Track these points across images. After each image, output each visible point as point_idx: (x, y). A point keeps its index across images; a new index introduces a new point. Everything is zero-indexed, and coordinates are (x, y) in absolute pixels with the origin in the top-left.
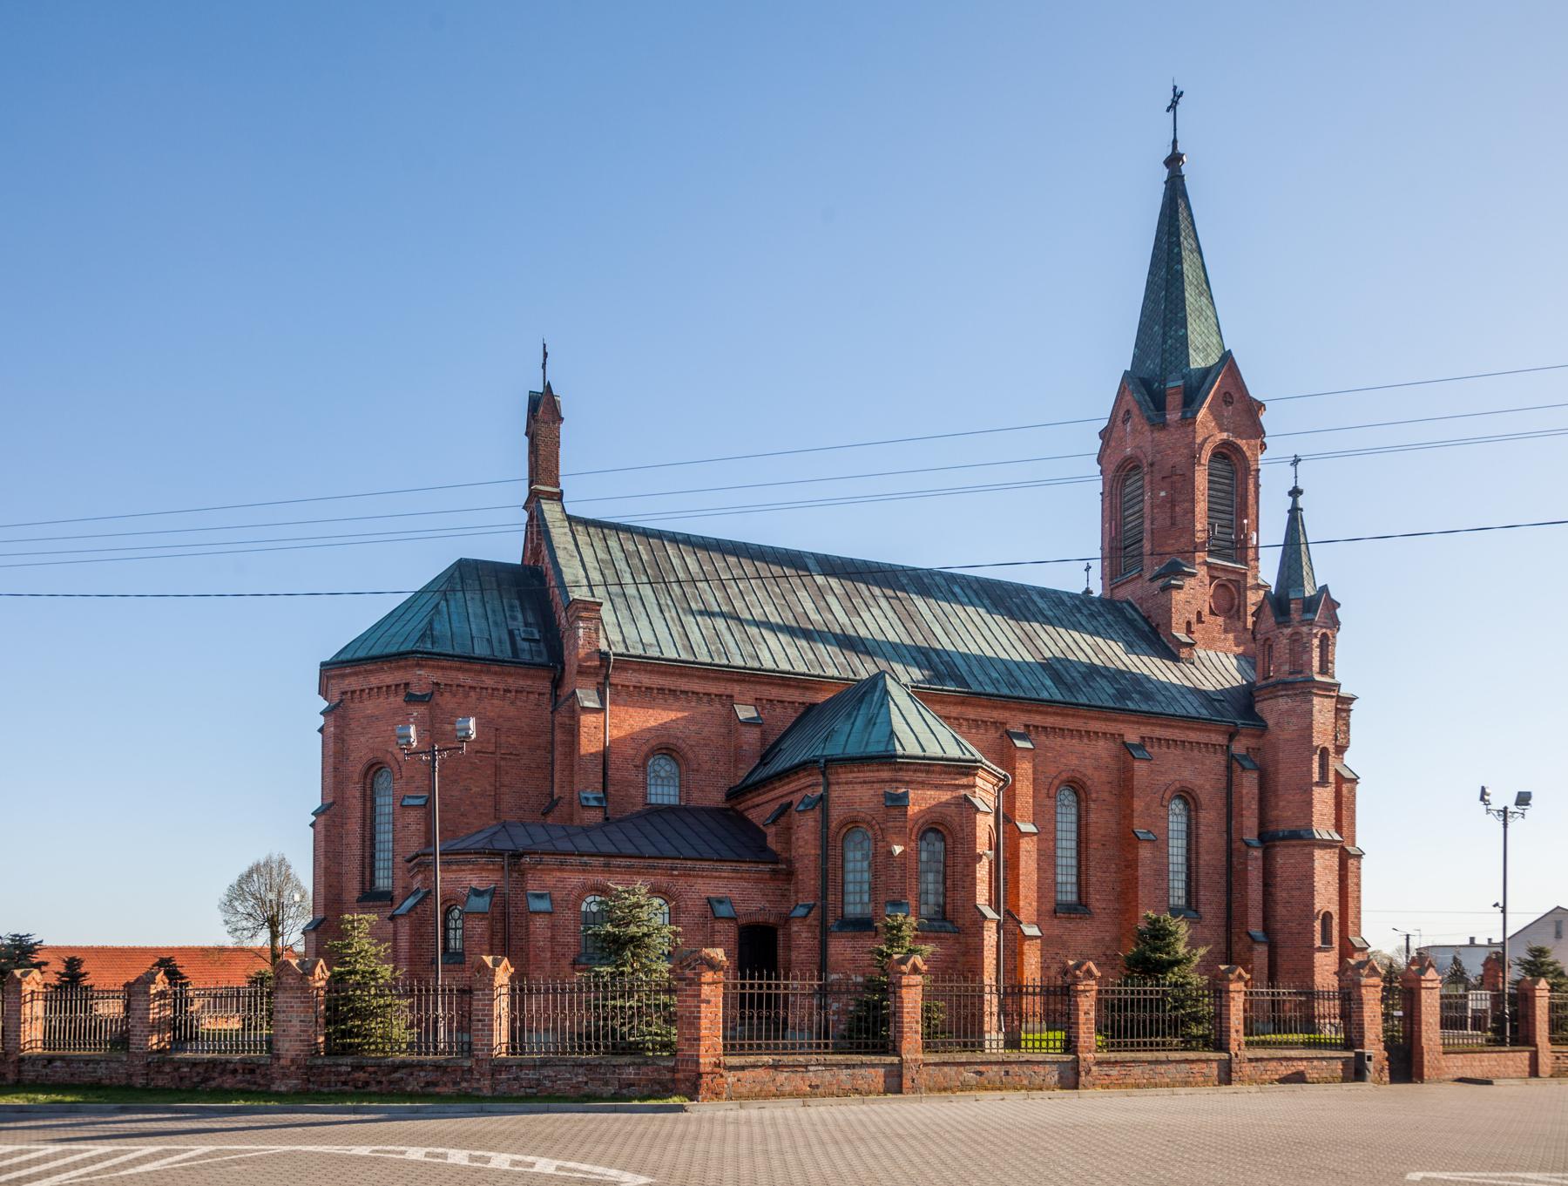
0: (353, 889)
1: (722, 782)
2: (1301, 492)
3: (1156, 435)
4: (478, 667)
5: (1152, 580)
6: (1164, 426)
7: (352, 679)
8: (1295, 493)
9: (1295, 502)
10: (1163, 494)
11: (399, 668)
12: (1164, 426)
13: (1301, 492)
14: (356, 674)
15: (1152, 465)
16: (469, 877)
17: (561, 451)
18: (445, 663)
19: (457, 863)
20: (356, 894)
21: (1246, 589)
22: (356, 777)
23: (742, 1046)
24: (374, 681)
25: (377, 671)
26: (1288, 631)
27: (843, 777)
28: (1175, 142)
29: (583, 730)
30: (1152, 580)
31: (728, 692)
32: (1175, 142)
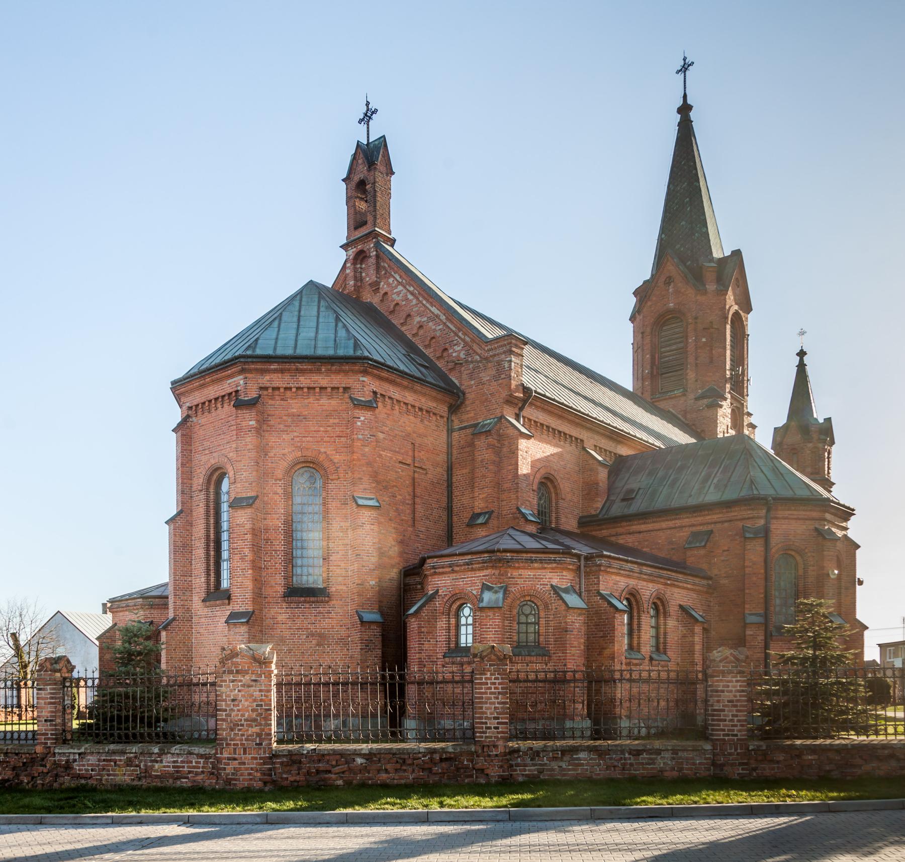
0: (277, 584)
1: (576, 512)
2: (805, 353)
3: (699, 297)
4: (405, 383)
5: (697, 399)
6: (705, 292)
7: (275, 376)
8: (802, 354)
9: (801, 360)
10: (704, 340)
11: (338, 372)
12: (705, 292)
13: (805, 353)
14: (282, 371)
15: (696, 318)
16: (549, 575)
17: (392, 201)
18: (384, 374)
19: (541, 561)
20: (281, 590)
21: (743, 415)
22: (279, 473)
23: (97, 735)
24: (304, 381)
25: (311, 371)
26: (810, 445)
27: (781, 514)
28: (685, 96)
29: (520, 453)
30: (697, 399)
31: (581, 437)
32: (685, 96)
